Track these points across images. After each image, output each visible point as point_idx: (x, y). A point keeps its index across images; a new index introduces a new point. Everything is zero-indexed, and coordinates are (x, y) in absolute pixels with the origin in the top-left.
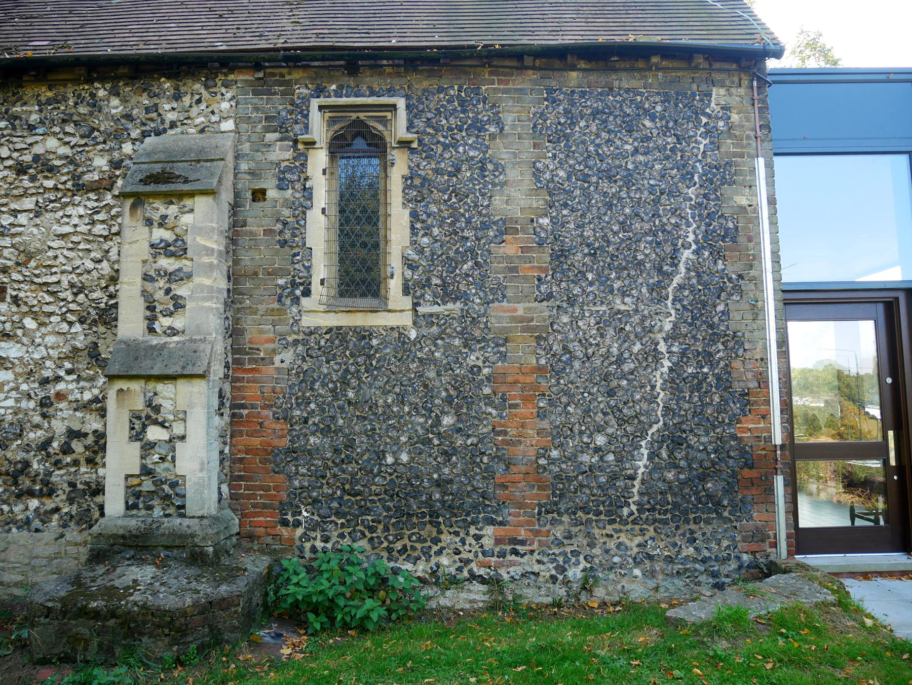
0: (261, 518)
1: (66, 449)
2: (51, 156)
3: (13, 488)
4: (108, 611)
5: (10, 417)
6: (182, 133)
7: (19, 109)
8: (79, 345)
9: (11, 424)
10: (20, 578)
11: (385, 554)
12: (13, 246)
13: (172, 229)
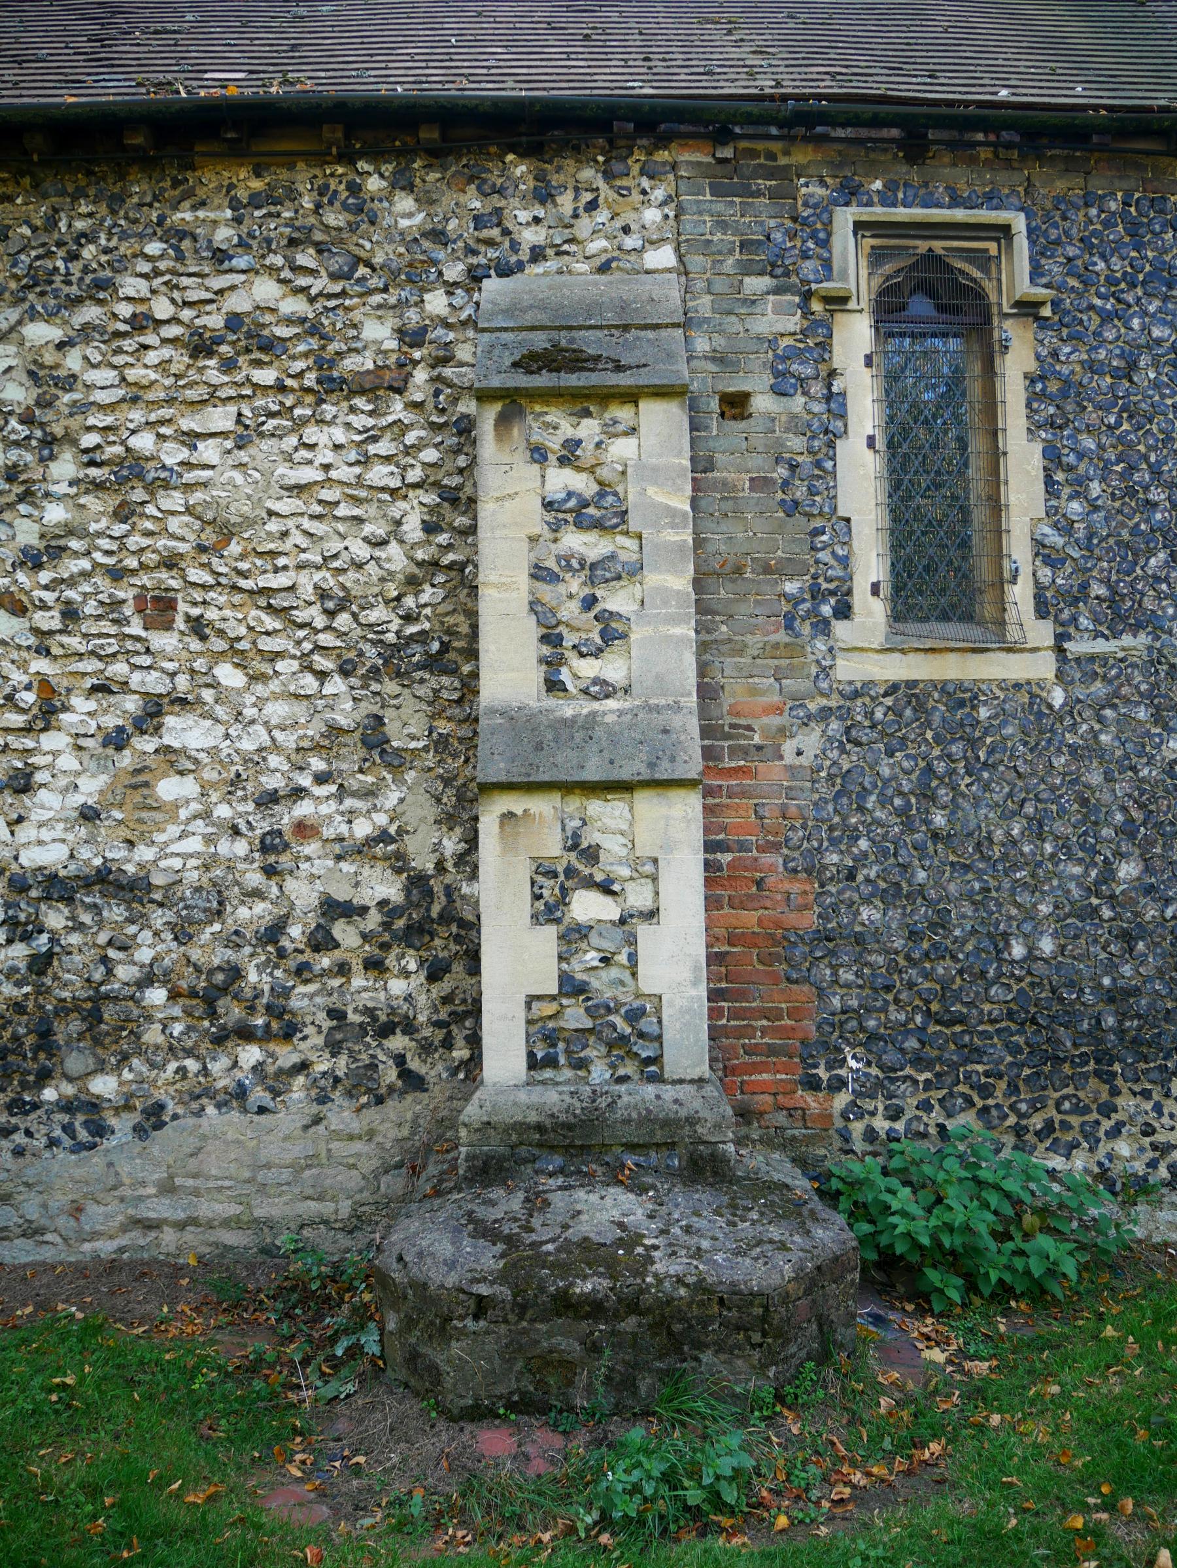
0: (765, 1076)
1: (321, 941)
2: (268, 318)
3: (206, 1023)
4: (620, 1300)
5: (195, 875)
6: (560, 272)
7: (188, 216)
8: (343, 722)
9: (198, 889)
10: (234, 1209)
11: (1009, 1140)
12: (189, 510)
13: (591, 470)
